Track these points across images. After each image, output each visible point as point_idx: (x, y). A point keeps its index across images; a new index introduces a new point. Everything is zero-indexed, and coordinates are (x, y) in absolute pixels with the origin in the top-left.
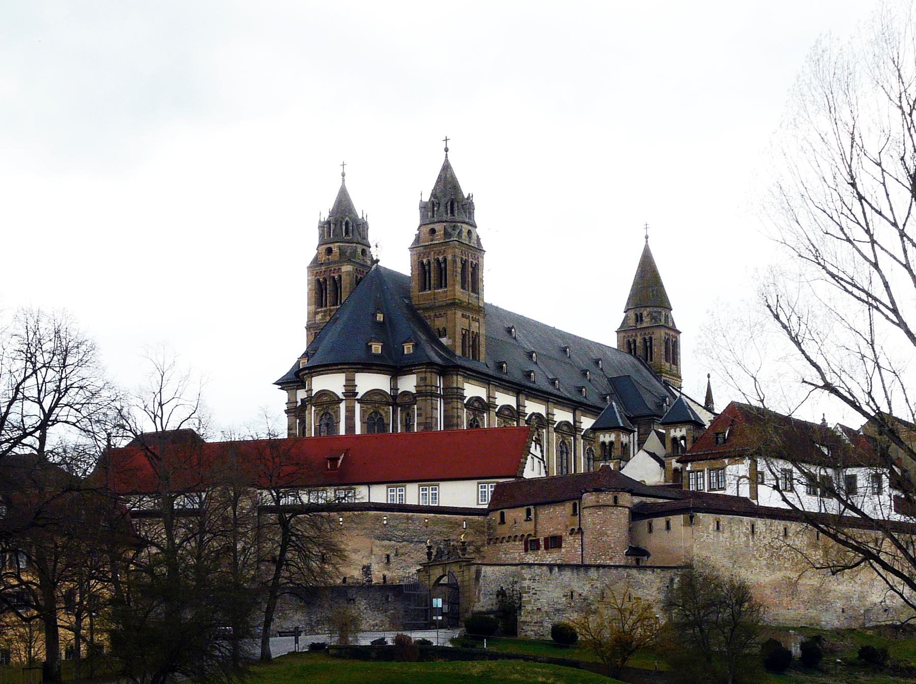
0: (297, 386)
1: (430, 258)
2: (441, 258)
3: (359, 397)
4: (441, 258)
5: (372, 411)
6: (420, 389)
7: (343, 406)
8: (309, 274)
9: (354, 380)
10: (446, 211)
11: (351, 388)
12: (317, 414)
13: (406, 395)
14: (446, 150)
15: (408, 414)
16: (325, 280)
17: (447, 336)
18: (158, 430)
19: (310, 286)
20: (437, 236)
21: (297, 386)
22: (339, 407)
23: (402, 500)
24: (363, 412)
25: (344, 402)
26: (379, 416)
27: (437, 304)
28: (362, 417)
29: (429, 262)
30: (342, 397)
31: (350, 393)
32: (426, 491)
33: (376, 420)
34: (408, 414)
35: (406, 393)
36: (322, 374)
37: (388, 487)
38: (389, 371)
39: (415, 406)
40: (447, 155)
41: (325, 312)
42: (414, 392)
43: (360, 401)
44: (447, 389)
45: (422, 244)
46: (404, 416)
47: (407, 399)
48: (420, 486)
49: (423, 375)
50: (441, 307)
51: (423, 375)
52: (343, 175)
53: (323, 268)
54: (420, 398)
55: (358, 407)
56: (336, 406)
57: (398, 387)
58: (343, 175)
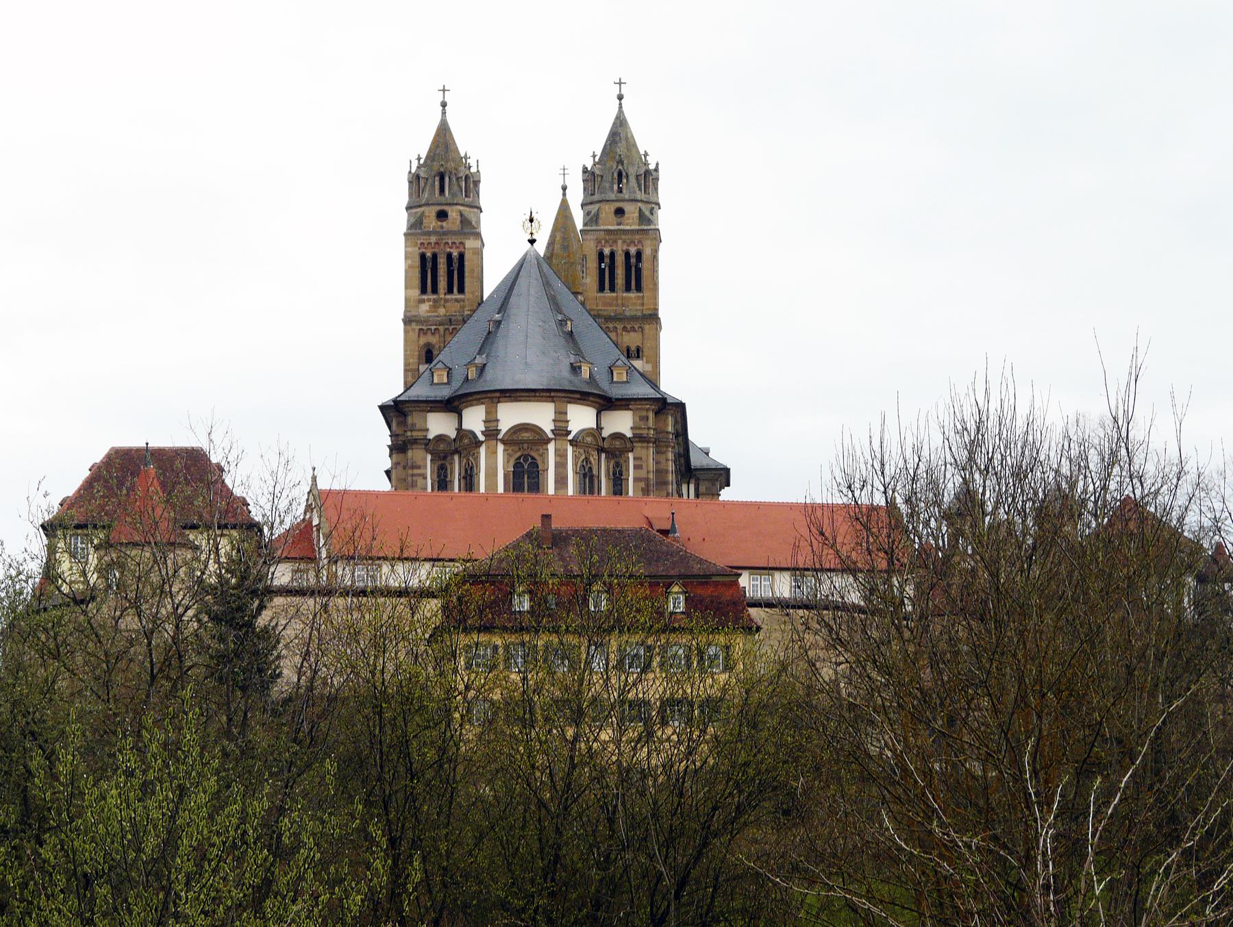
0: (431, 407)
1: (614, 248)
2: (633, 250)
3: (570, 437)
4: (633, 250)
5: (519, 454)
6: (637, 432)
7: (551, 447)
8: (409, 244)
9: (566, 414)
10: (639, 186)
11: (563, 424)
12: (510, 455)
13: (621, 438)
14: (620, 97)
15: (617, 465)
16: (435, 256)
17: (644, 358)
18: (686, 485)
19: (409, 262)
20: (628, 219)
21: (431, 407)
22: (547, 450)
23: (757, 592)
24: (576, 458)
25: (553, 442)
26: (589, 465)
27: (628, 314)
28: (575, 464)
29: (612, 254)
30: (551, 435)
31: (561, 431)
32: (757, 581)
33: (526, 467)
34: (617, 465)
35: (618, 436)
36: (520, 401)
37: (750, 574)
38: (594, 402)
39: (631, 455)
40: (620, 104)
41: (435, 301)
42: (629, 434)
43: (573, 443)
44: (490, 421)
45: (602, 227)
46: (611, 466)
47: (617, 444)
48: (750, 574)
49: (644, 413)
50: (634, 318)
51: (644, 413)
52: (444, 105)
53: (433, 239)
54: (639, 444)
55: (501, 447)
56: (544, 447)
57: (499, 418)
58: (444, 105)
